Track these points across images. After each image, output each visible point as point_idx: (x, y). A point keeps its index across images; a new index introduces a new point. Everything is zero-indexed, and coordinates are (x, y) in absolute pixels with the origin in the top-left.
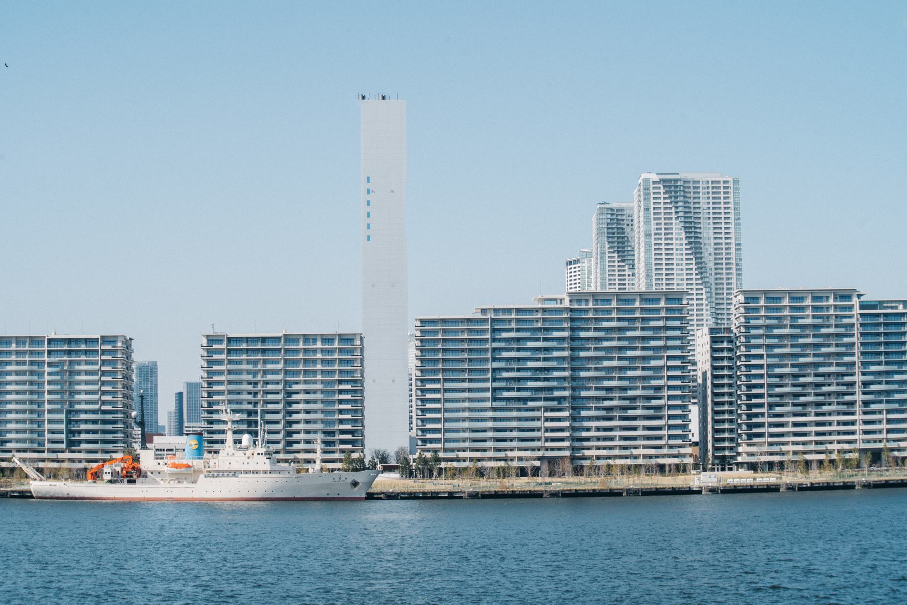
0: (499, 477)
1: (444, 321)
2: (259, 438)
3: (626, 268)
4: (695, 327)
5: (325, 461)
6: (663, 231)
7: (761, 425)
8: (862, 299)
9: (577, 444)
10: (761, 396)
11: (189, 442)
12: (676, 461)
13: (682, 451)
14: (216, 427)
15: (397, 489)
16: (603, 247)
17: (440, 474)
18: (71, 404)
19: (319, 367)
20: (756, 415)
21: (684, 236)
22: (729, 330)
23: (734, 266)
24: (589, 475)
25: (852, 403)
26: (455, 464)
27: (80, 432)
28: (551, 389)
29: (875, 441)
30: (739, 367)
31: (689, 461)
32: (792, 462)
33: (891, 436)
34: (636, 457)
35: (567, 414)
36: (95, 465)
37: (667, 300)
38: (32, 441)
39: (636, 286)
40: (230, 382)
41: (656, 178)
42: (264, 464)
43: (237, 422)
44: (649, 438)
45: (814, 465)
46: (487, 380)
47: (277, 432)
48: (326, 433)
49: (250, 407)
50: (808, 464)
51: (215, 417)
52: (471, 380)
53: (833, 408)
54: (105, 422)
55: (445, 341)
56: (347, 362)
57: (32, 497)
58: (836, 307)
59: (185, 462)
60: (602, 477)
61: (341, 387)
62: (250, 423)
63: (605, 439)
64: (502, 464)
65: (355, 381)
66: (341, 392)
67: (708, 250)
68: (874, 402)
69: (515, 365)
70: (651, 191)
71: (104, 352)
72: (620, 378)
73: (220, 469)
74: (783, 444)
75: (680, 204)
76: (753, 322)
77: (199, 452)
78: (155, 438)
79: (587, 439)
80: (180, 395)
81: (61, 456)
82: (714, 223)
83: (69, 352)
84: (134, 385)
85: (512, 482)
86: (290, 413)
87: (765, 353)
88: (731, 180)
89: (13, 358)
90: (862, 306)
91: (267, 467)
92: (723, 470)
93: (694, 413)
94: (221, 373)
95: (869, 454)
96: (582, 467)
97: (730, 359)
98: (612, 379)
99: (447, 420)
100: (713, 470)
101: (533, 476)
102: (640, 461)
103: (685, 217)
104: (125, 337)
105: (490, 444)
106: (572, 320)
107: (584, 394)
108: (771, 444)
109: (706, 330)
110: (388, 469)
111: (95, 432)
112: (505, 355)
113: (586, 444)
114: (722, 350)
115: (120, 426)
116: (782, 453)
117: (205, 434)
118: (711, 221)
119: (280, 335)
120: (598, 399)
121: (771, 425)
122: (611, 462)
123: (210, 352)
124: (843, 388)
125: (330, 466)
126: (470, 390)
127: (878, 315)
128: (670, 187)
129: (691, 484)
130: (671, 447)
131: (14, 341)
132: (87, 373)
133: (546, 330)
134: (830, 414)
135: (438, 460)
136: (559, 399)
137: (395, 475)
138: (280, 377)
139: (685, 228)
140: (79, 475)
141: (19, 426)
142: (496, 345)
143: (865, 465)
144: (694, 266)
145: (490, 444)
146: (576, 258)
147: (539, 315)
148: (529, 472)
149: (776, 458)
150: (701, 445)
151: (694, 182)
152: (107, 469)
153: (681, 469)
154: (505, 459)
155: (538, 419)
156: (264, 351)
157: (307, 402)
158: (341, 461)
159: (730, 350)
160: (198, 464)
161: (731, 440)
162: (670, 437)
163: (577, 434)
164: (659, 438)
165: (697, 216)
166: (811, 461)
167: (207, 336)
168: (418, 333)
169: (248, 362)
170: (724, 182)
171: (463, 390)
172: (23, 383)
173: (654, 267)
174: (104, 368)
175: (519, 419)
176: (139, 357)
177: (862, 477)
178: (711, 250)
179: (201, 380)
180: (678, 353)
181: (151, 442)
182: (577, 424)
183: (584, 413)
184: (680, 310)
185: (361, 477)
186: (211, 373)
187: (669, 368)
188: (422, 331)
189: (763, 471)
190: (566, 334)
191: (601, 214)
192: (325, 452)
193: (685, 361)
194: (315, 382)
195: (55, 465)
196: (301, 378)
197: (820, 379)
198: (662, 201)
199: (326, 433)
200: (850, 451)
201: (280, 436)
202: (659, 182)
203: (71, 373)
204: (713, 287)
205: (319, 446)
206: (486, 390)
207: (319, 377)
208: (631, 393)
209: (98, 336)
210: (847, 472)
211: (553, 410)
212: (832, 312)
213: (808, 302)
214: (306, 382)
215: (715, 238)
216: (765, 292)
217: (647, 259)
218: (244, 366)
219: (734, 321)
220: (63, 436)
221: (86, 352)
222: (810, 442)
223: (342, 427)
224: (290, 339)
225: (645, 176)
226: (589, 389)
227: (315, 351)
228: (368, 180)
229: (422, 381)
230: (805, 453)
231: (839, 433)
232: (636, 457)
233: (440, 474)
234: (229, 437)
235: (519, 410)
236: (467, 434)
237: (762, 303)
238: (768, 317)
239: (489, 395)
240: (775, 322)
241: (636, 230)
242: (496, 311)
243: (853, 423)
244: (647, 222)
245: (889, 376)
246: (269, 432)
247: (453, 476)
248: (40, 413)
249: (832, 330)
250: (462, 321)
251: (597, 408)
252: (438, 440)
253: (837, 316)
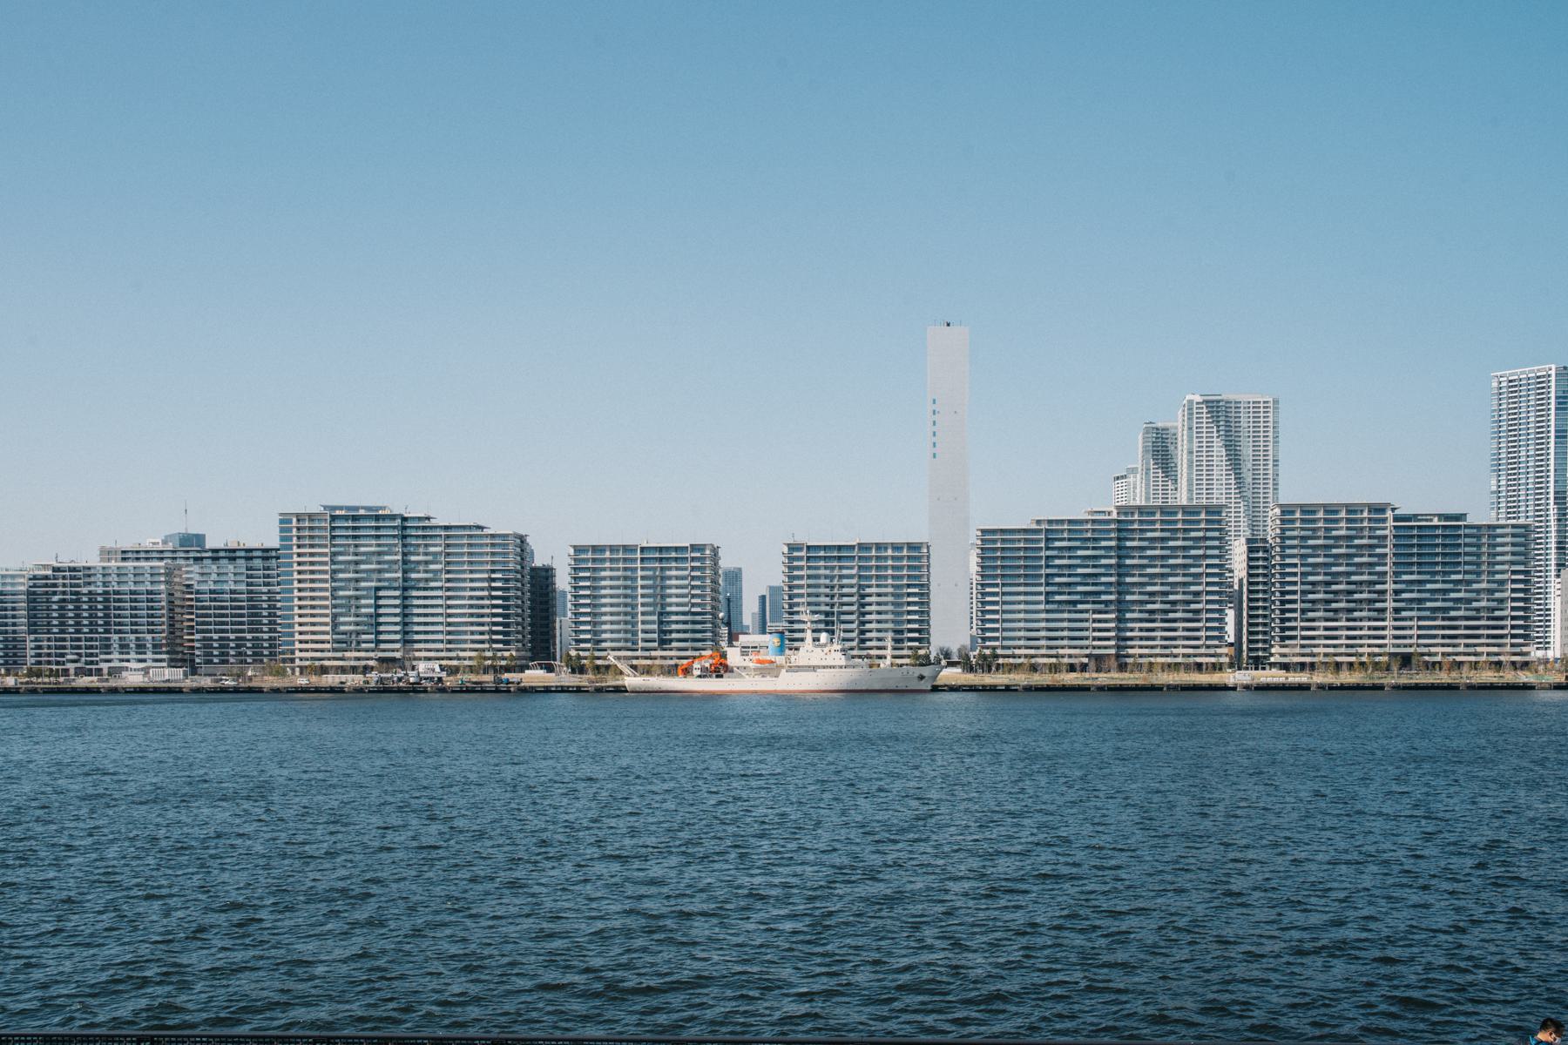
0: (1050, 672)
1: (1003, 531)
2: (836, 636)
3: (1169, 483)
4: (1233, 538)
5: (894, 657)
6: (1204, 449)
8: (1396, 512)
9: (1122, 643)
10: (1294, 602)
11: (771, 640)
12: (1213, 660)
13: (1219, 651)
14: (796, 626)
15: (959, 683)
16: (1148, 463)
17: (997, 669)
18: (663, 606)
19: (890, 572)
20: (1289, 620)
21: (1224, 454)
22: (1265, 541)
23: (1271, 481)
24: (1132, 672)
25: (1383, 610)
26: (1011, 660)
27: (671, 632)
28: (1099, 593)
29: (1405, 646)
30: (1273, 575)
31: (1225, 660)
32: (1323, 663)
33: (1421, 641)
34: (1176, 656)
35: (1113, 616)
36: (685, 662)
37: (1207, 513)
38: (626, 640)
39: (1178, 500)
40: (809, 586)
41: (1200, 399)
42: (840, 659)
43: (816, 622)
44: (1188, 638)
45: (1344, 667)
46: (1041, 585)
47: (852, 631)
48: (896, 631)
49: (828, 609)
50: (1338, 666)
51: (796, 617)
52: (1026, 585)
53: (1364, 614)
54: (694, 622)
55: (1003, 549)
56: (915, 568)
57: (627, 691)
58: (1370, 519)
59: (768, 658)
60: (1145, 674)
61: (910, 590)
62: (827, 623)
63: (1148, 639)
64: (1053, 660)
65: (922, 585)
66: (909, 595)
67: (1247, 466)
68: (1404, 609)
69: (1066, 572)
70: (1195, 411)
71: (693, 559)
72: (1162, 584)
73: (801, 664)
74: (1315, 646)
75: (1221, 423)
76: (1288, 533)
77: (781, 650)
78: (741, 637)
79: (1131, 639)
80: (763, 598)
81: (653, 653)
83: (661, 560)
84: (721, 589)
85: (1062, 677)
86: (864, 614)
89: (607, 565)
90: (1396, 519)
91: (843, 662)
92: (1256, 669)
93: (1230, 616)
94: (801, 577)
95: (1399, 658)
96: (1126, 664)
97: (1265, 567)
98: (1155, 584)
99: (1004, 603)
100: (1247, 669)
101: (1082, 671)
102: (1179, 660)
103: (1226, 436)
104: (712, 545)
105: (1043, 642)
106: (1119, 530)
107: (1129, 598)
108: (1303, 646)
109: (1243, 540)
110: (951, 664)
111: (685, 631)
112: (1057, 562)
113: (1129, 643)
114: (1257, 559)
115: (709, 626)
116: (1314, 655)
117: (787, 633)
118: (1251, 439)
119: (854, 543)
120: (1142, 602)
121: (1303, 629)
122: (1152, 660)
123: (791, 559)
124: (1375, 596)
125: (899, 661)
126: (1026, 594)
127: (1412, 527)
128: (1213, 407)
129: (1227, 681)
130: (1208, 647)
131: (608, 549)
132: (677, 578)
133: (1095, 539)
134: (1361, 620)
135: (997, 656)
136: (1106, 603)
137: (958, 670)
138: (854, 581)
139: (1226, 446)
140: (671, 671)
141: (615, 627)
142: (1049, 553)
143: (1395, 668)
144: (1233, 482)
145: (1043, 642)
146: (1123, 474)
147: (1089, 526)
148: (1078, 669)
149: (1308, 660)
150: (1237, 645)
151: (1236, 402)
152: (696, 665)
153: (1217, 667)
154: (1056, 656)
155: (1087, 620)
156: (840, 558)
157: (879, 604)
158: (909, 657)
159: (1265, 559)
160: (780, 659)
161: (1265, 641)
162: (1208, 638)
163: (1122, 634)
164: (1197, 638)
166: (1342, 663)
167: (788, 545)
168: (979, 542)
169: (826, 568)
170: (1264, 402)
171: (1019, 594)
172: (618, 587)
173: (1195, 482)
174: (693, 574)
175: (1070, 620)
176: (726, 563)
177: (1391, 679)
178: (1250, 466)
179: (782, 584)
180: (1216, 561)
181: (737, 640)
182: (1122, 625)
183: (1128, 615)
184: (1219, 522)
185: (926, 671)
186: (792, 578)
187: (1208, 575)
188: (982, 540)
189: (1295, 671)
190: (1113, 543)
191: (1147, 433)
192: (895, 649)
193: (1223, 569)
194: (886, 586)
195: (649, 662)
196: (874, 582)
197: (1353, 587)
198: (1204, 420)
199: (896, 631)
200: (1380, 655)
201: (854, 635)
202: (1202, 403)
203: (663, 578)
204: (1251, 501)
205: (889, 643)
206: (1040, 593)
207: (890, 581)
208: (1172, 597)
209: (687, 545)
210: (1377, 674)
211: (1100, 612)
212: (1365, 524)
213: (1343, 515)
214: (878, 586)
216: (1301, 506)
217: (1189, 474)
218: (822, 572)
219: (1270, 532)
220: (656, 636)
221: (676, 559)
222: (1341, 645)
223: (910, 626)
224: (863, 547)
226: (1133, 593)
227: (886, 558)
228: (934, 401)
229: (982, 585)
230: (1335, 655)
231: (1369, 637)
232: (1176, 656)
233: (997, 669)
234: (809, 635)
235: (1070, 612)
236: (1022, 634)
237: (1298, 515)
238: (1302, 529)
239: (1042, 598)
240: (1310, 533)
241: (1180, 448)
242: (1050, 522)
243: (1383, 628)
244: (1190, 440)
246: (845, 631)
247: (1010, 672)
248: (634, 615)
249: (1365, 541)
250: (1019, 531)
251: (1141, 611)
252: (996, 639)
253: (1370, 528)
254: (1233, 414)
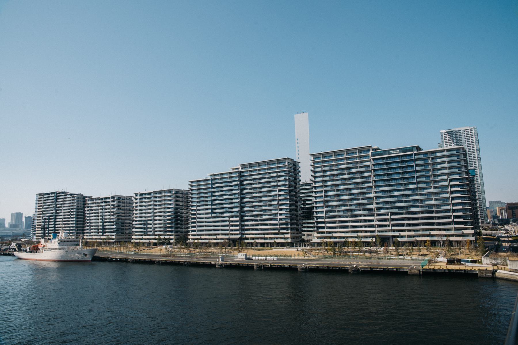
7: (323, 222)
23: (476, 157)
41: (445, 131)
70: (444, 136)
75: (454, 139)
82: (467, 143)
87: (323, 185)
88: (473, 128)
113: (246, 232)
118: (466, 143)
151: (459, 131)
165: (461, 142)
170: (470, 129)
183: (246, 218)
215: (468, 148)
225: (441, 131)
239: (210, 211)
245: (421, 191)
254: (458, 135)
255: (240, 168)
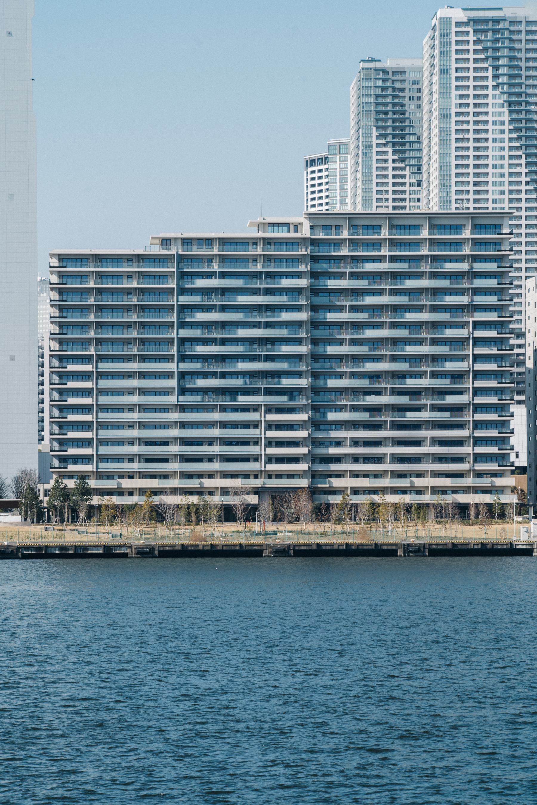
41: (462, 17)
75: (502, 62)
139: (510, 104)
144: (523, 170)
151: (528, 23)
183: (332, 416)
225: (442, 13)
239: (173, 383)
254: (523, 46)
255: (306, 225)
